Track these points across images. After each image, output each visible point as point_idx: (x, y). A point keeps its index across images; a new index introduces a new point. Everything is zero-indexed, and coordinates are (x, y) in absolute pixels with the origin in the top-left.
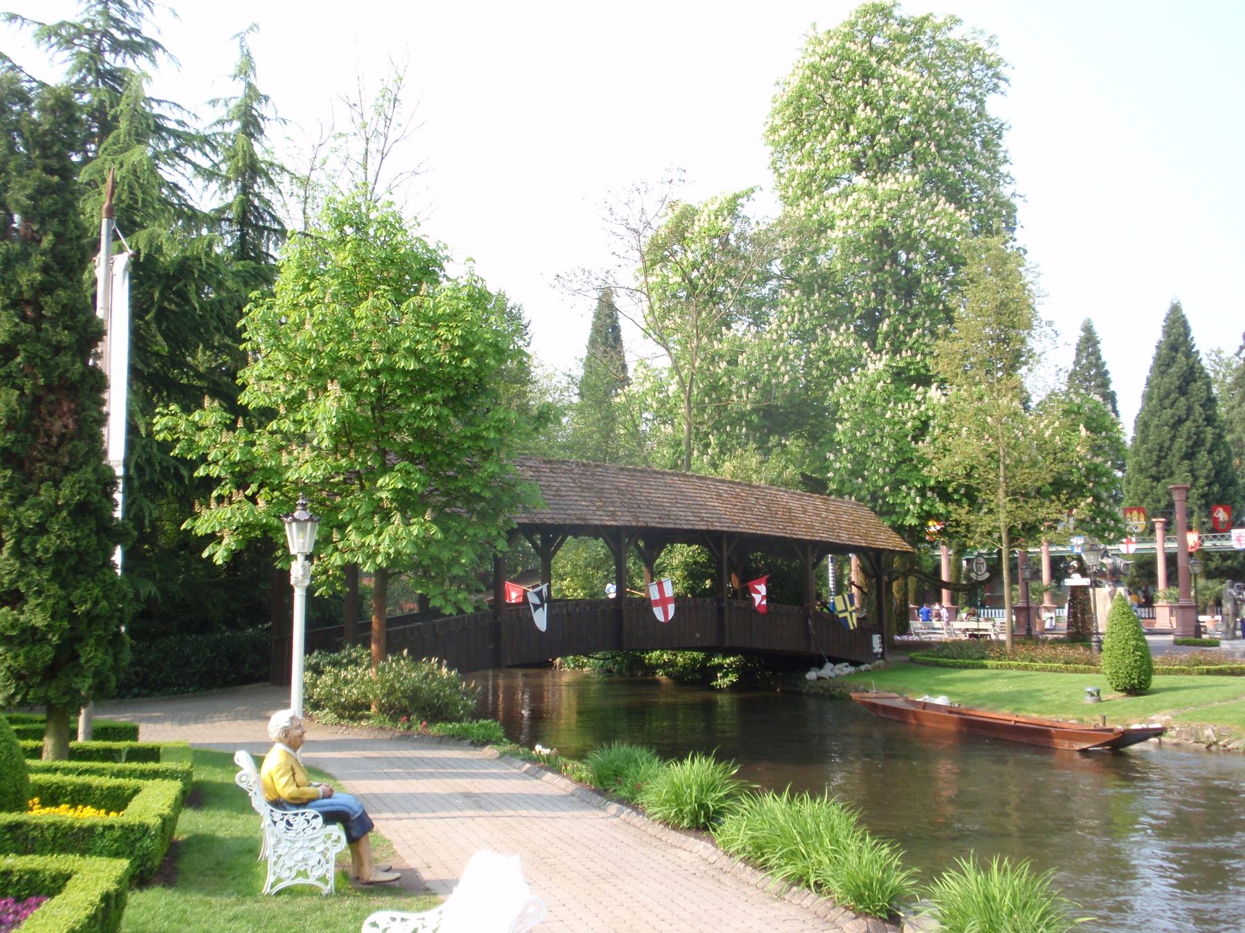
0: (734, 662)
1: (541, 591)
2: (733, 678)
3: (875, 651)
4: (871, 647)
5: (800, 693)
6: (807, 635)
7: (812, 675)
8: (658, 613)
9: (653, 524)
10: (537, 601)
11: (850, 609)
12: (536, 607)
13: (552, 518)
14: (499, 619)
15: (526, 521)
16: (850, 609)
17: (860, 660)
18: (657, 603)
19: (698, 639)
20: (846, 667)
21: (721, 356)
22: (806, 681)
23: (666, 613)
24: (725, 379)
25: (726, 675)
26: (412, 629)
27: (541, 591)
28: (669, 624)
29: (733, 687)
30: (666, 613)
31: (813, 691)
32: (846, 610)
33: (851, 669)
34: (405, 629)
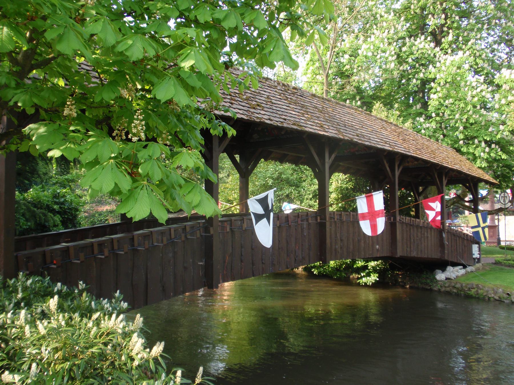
0: (378, 265)
1: (266, 197)
2: (374, 278)
3: (474, 257)
4: (471, 254)
5: (431, 290)
6: (442, 245)
7: (440, 276)
8: (365, 227)
9: (356, 140)
10: (260, 211)
11: (482, 225)
12: (259, 217)
13: (269, 119)
14: (212, 232)
15: (245, 117)
16: (482, 225)
17: (494, 266)
18: (364, 217)
19: (378, 250)
20: (461, 269)
21: (345, 52)
22: (437, 281)
23: (374, 227)
24: (348, 67)
25: (368, 275)
26: (101, 245)
27: (266, 197)
28: (375, 238)
29: (375, 285)
30: (374, 227)
31: (443, 289)
32: (479, 226)
33: (463, 271)
34: (92, 244)
